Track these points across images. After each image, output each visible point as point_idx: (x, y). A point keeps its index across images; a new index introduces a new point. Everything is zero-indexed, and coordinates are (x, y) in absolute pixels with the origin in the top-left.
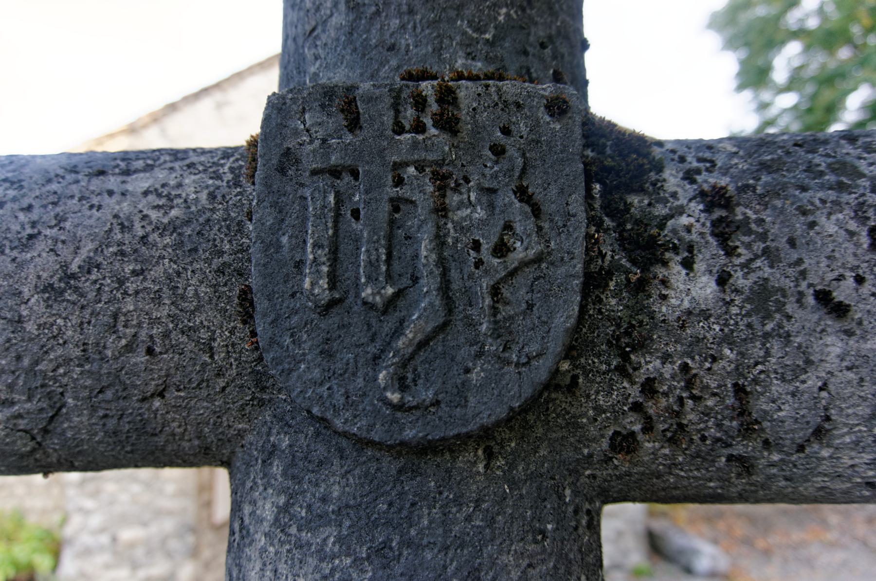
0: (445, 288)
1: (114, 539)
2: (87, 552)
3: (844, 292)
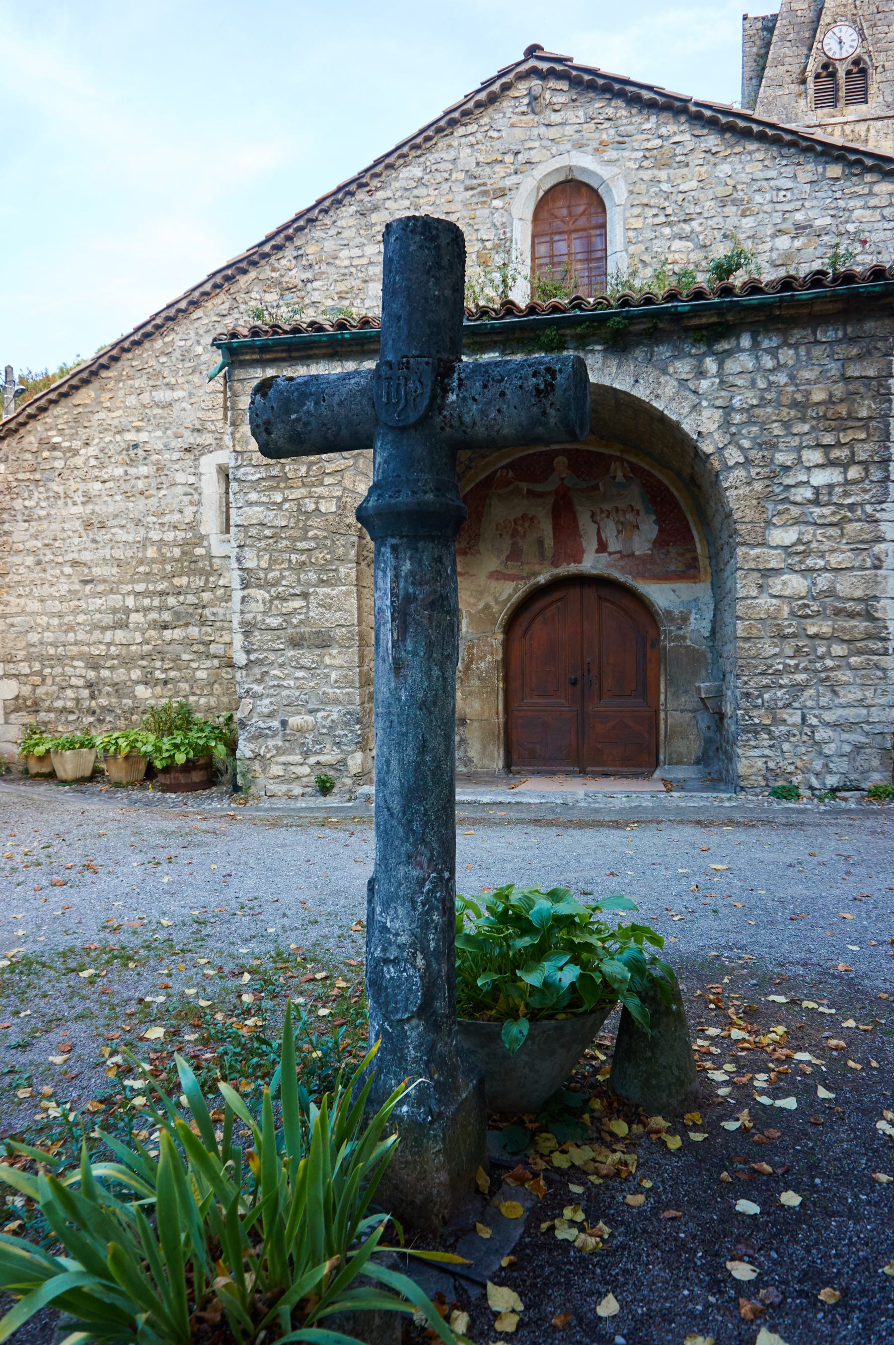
0: (406, 399)
1: (284, 723)
2: (260, 735)
3: (477, 397)
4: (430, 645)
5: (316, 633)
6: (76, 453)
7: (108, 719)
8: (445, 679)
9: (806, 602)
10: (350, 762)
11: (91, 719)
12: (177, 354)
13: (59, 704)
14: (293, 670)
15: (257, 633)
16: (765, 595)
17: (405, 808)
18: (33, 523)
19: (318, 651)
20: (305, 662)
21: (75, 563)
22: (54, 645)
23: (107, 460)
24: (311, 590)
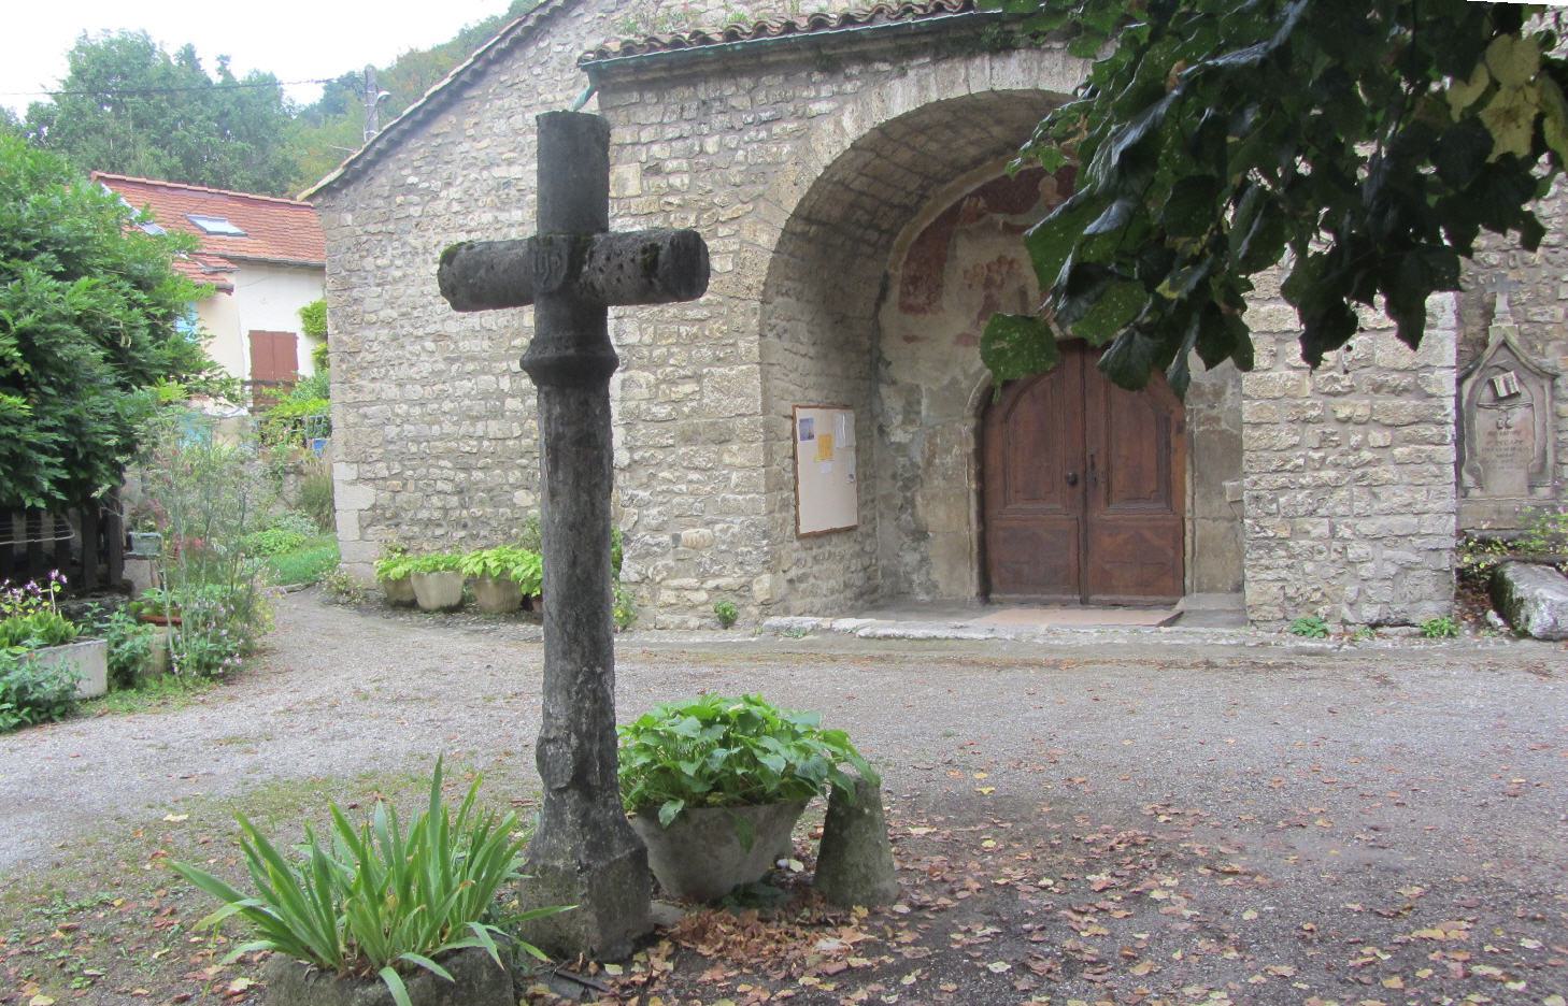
1: (676, 538)
4: (578, 476)
5: (712, 424)
6: (435, 197)
7: (482, 533)
8: (593, 505)
9: (1335, 375)
10: (756, 587)
11: (463, 533)
12: (554, 63)
13: (424, 514)
14: (686, 471)
15: (641, 426)
16: (1281, 366)
17: (561, 612)
18: (387, 287)
19: (714, 448)
20: (700, 461)
21: (439, 337)
22: (416, 441)
23: (473, 203)
24: (705, 371)
